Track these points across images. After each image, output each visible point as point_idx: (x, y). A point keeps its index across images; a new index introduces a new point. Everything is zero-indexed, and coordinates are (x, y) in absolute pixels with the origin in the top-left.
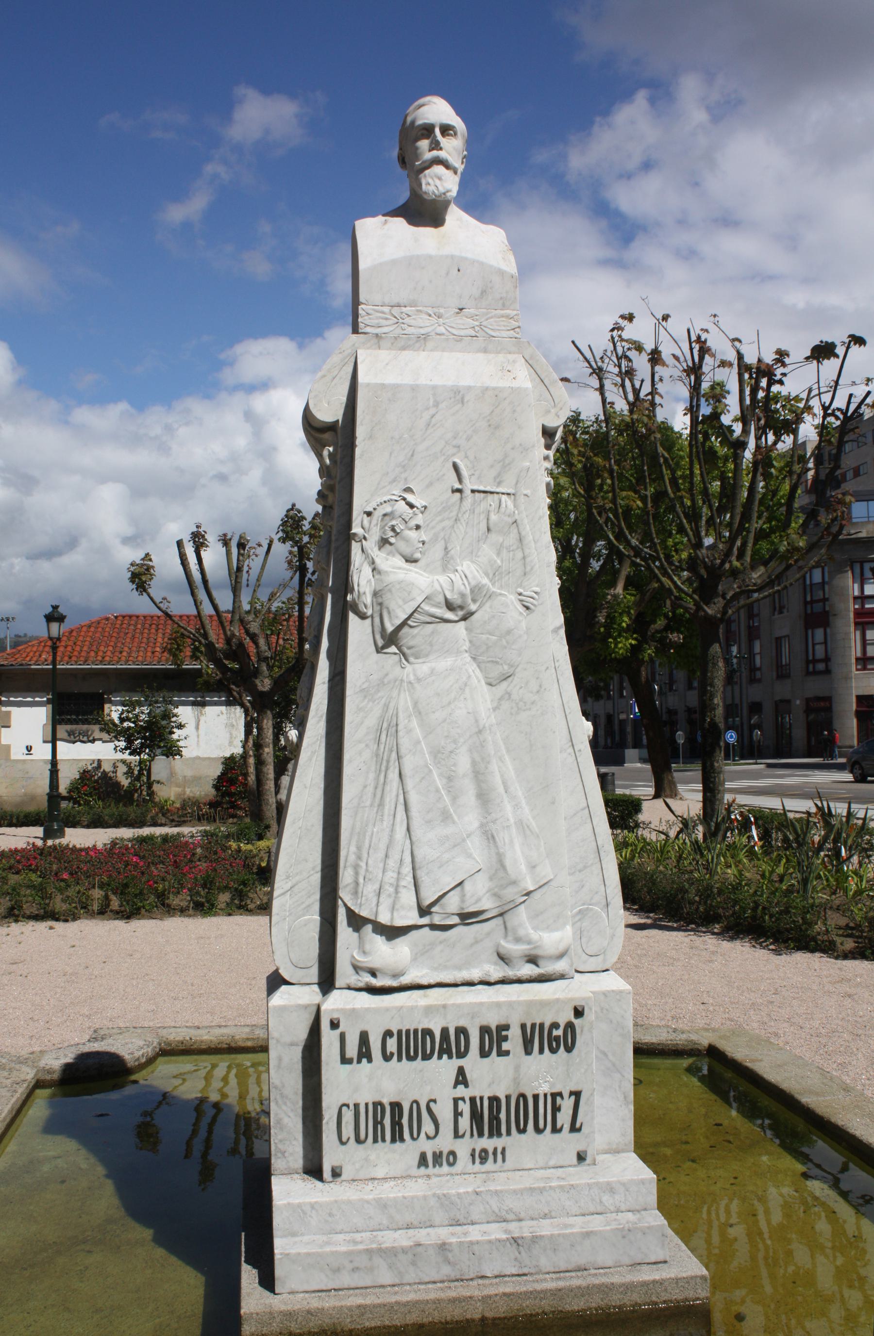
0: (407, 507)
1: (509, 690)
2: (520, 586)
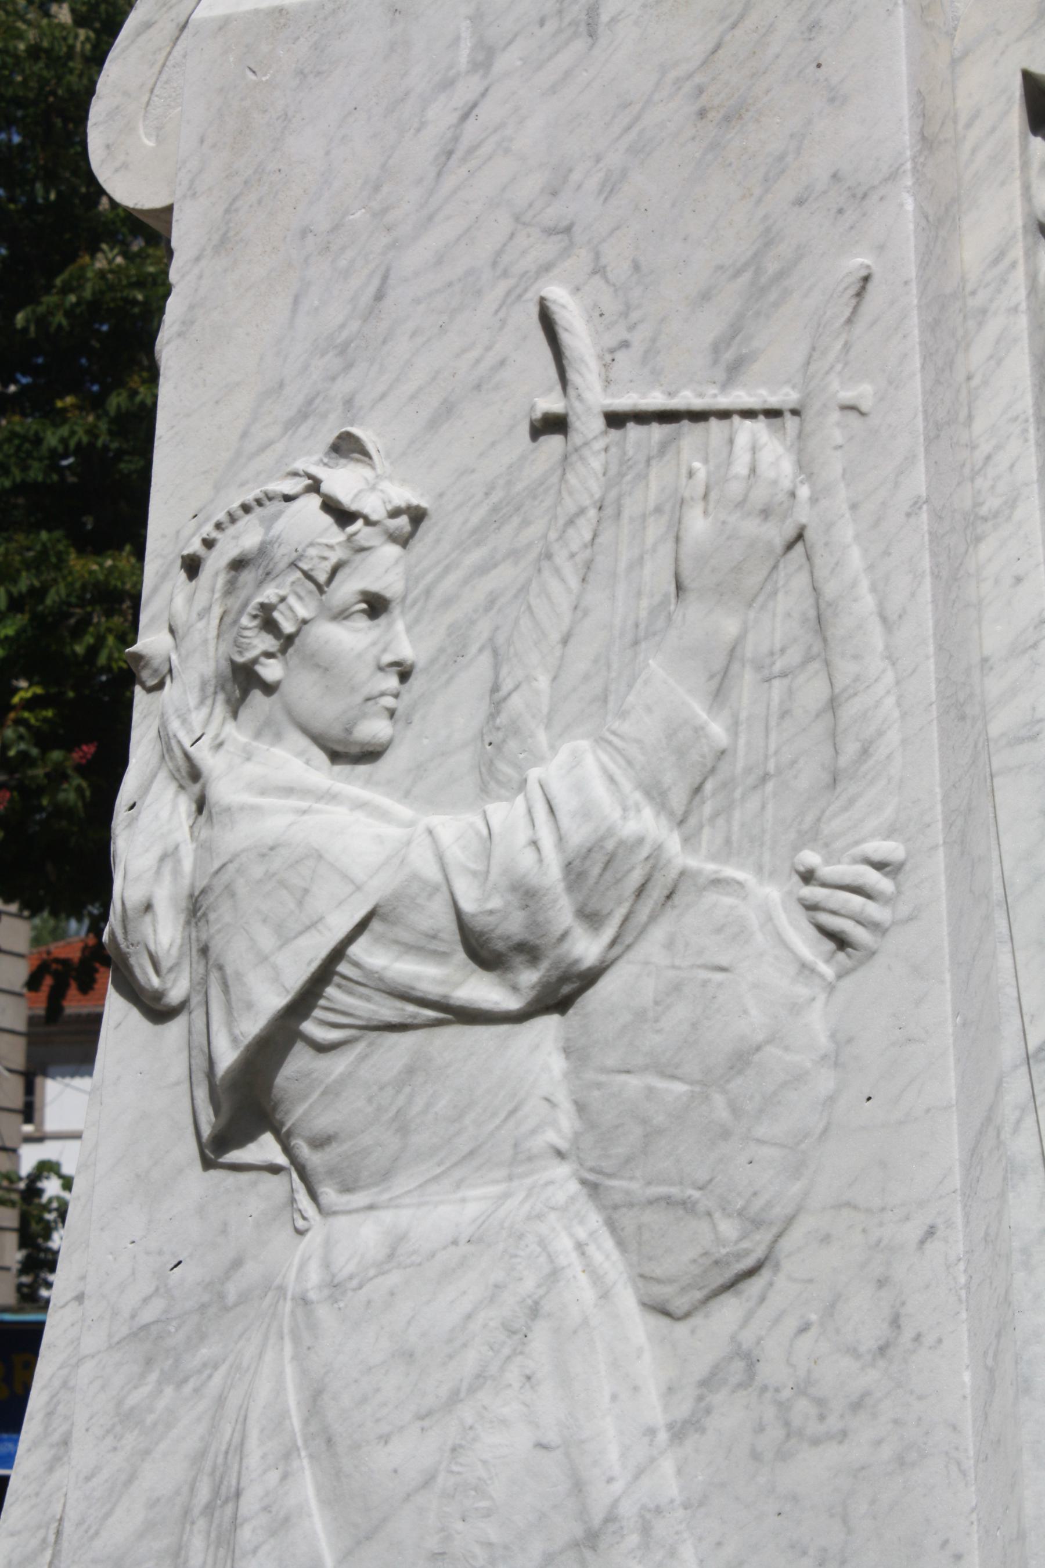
0: (327, 520)
1: (747, 1337)
2: (810, 837)
